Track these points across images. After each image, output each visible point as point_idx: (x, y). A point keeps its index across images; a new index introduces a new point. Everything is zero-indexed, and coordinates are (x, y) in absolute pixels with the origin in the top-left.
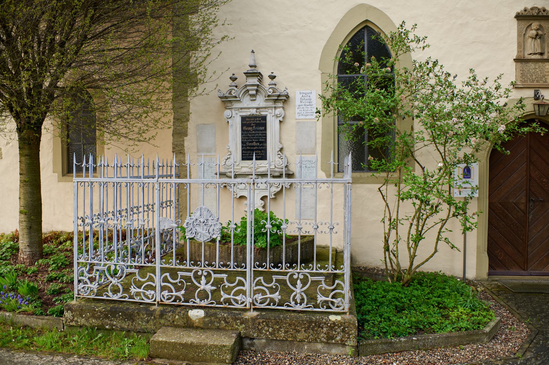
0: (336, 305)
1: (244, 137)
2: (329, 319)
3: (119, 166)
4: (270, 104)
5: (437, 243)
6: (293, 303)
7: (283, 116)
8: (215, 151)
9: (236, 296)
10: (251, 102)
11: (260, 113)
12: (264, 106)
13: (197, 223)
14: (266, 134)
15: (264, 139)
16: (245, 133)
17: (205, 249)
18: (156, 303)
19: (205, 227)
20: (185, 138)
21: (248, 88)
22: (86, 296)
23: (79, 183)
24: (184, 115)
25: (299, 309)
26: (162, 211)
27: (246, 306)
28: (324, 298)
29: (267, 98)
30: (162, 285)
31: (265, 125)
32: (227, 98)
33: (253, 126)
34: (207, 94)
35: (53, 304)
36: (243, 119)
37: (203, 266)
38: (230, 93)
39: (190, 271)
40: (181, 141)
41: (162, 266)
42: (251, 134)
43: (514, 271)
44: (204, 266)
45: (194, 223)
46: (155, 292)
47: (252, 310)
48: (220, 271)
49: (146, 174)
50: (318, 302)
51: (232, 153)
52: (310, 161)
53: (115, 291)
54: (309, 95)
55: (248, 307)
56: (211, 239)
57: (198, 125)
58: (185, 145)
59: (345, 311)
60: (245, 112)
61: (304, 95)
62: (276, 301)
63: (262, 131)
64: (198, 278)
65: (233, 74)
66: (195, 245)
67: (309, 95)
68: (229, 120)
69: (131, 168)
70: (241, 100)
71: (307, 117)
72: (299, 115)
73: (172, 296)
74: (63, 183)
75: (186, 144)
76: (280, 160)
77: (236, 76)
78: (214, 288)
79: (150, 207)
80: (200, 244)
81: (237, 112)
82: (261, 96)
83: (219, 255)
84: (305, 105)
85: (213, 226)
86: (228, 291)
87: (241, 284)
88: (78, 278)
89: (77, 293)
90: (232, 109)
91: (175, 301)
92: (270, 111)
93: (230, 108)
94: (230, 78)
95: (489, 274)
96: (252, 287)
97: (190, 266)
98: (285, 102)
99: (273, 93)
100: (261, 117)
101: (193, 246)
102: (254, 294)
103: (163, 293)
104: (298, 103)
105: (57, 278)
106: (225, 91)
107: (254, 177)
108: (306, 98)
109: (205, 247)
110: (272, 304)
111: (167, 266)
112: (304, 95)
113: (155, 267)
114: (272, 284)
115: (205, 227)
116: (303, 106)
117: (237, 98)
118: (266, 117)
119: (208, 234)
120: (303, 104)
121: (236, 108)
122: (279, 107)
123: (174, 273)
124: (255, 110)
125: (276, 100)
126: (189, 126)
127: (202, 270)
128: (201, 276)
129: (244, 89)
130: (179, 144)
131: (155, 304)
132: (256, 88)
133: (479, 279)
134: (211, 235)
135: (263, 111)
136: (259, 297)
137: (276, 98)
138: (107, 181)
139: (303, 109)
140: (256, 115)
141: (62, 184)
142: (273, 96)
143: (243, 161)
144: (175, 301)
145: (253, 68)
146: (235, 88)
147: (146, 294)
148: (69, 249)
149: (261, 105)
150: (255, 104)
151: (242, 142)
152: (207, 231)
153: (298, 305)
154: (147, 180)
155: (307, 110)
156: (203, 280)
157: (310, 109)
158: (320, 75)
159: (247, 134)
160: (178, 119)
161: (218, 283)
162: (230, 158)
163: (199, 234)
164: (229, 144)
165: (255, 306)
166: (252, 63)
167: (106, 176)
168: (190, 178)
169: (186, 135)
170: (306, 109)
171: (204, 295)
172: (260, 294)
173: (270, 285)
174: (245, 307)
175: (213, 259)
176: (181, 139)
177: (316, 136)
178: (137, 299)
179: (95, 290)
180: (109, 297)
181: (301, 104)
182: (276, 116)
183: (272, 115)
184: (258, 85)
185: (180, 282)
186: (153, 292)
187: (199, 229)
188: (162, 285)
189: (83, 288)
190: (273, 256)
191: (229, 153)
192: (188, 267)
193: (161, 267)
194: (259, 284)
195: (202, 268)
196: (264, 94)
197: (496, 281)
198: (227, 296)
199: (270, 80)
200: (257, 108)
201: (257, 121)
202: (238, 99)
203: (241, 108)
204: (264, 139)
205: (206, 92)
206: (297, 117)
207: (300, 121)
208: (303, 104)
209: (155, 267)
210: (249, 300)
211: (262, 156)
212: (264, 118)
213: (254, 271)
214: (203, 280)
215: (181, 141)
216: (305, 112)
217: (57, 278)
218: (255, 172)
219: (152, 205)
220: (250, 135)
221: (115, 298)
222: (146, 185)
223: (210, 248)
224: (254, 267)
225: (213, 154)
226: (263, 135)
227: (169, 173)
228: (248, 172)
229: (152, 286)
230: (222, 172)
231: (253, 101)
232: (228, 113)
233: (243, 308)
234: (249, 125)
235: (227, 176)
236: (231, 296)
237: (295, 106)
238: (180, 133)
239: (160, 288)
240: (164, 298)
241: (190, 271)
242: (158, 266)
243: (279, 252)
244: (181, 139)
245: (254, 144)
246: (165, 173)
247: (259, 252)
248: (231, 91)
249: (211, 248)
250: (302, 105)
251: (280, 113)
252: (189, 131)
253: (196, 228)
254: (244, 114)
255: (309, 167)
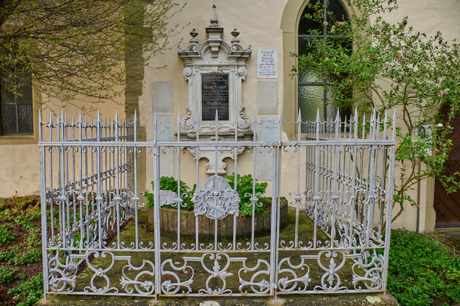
0: (372, 284)
1: (204, 96)
2: (368, 302)
3: (85, 126)
4: (233, 62)
6: (324, 286)
7: (245, 75)
8: (172, 111)
9: (256, 282)
10: (212, 59)
11: (221, 71)
12: (226, 64)
13: (209, 196)
14: (228, 93)
15: (226, 98)
16: (206, 92)
17: (181, 219)
18: (155, 296)
19: (220, 201)
21: (211, 44)
22: (60, 291)
23: (47, 149)
24: (138, 72)
25: (332, 292)
26: (121, 175)
27: (269, 292)
28: (360, 278)
29: (230, 56)
30: (163, 274)
32: (187, 55)
33: (214, 85)
34: (169, 49)
35: (9, 298)
37: (216, 248)
38: (191, 49)
39: (200, 255)
40: (135, 100)
41: (163, 251)
42: (212, 93)
43: (453, 223)
44: (218, 249)
45: (206, 197)
46: (154, 282)
47: (276, 297)
48: (240, 253)
49: (84, 138)
50: (353, 282)
51: (192, 113)
52: (272, 121)
53: (99, 282)
54: (270, 54)
55: (271, 294)
56: (227, 215)
57: (153, 84)
58: (139, 104)
59: (382, 290)
60: (206, 70)
61: (266, 54)
62: (304, 285)
64: (210, 264)
65: (194, 30)
66: (167, 214)
67: (270, 54)
68: (189, 78)
69: (84, 129)
70: (202, 58)
71: (269, 77)
72: (261, 75)
73: (176, 287)
75: (140, 103)
76: (243, 120)
77: (196, 31)
78: (230, 274)
79: (112, 172)
80: (213, 221)
81: (197, 69)
82: (223, 54)
83: (199, 224)
84: (267, 64)
85: (230, 200)
86: (247, 277)
87: (263, 267)
88: (48, 270)
89: (48, 289)
90: (192, 66)
91: (180, 292)
92: (233, 69)
93: (190, 66)
94: (191, 34)
95: (436, 227)
96: (277, 270)
97: (199, 249)
98: (247, 60)
99: (237, 50)
101: (165, 216)
102: (279, 278)
103: (164, 284)
104: (259, 62)
105: (6, 259)
106: (185, 48)
107: (217, 137)
108: (267, 57)
109: (181, 216)
110: (299, 288)
111: (170, 250)
112: (266, 54)
113: (154, 252)
114: (301, 265)
115: (220, 201)
116: (265, 65)
117: (198, 54)
118: (228, 75)
119: (223, 210)
120: (265, 63)
121: (196, 65)
122: (242, 66)
123: (177, 258)
124: (217, 68)
125: (239, 57)
126: (144, 85)
127: (215, 254)
128: (213, 261)
129: (205, 45)
130: (132, 103)
131: (154, 298)
132: (219, 44)
133: (427, 232)
134: (227, 210)
135: (225, 69)
136: (285, 281)
137: (240, 56)
138: (86, 145)
139: (264, 69)
140: (218, 73)
142: (237, 53)
143: (204, 121)
144: (180, 292)
145: (215, 24)
146: (196, 44)
147: (142, 286)
148: (9, 219)
149: (223, 63)
150: (217, 62)
152: (222, 206)
153: (330, 287)
154: (104, 143)
155: (269, 70)
156: (216, 266)
157: (271, 68)
158: (282, 35)
159: (208, 93)
160: (131, 77)
161: (235, 266)
162: (190, 118)
163: (212, 210)
164: (189, 104)
165: (280, 293)
166: (214, 19)
167: (65, 140)
168: (257, 140)
169: (141, 94)
170: (268, 68)
171: (216, 283)
172: (287, 278)
173: (298, 267)
174: (268, 295)
175: (191, 229)
176: (135, 98)
177: (277, 96)
178: (130, 293)
179: (74, 285)
180: (92, 291)
181: (262, 63)
182: (238, 75)
183: (234, 73)
184: (221, 41)
185: (187, 269)
186: (150, 283)
187: (211, 204)
188: (163, 274)
189: (56, 282)
190: (257, 223)
191: (189, 113)
192: (197, 251)
193: (161, 253)
194: (285, 266)
195: (215, 251)
196: (227, 51)
197: (443, 233)
198: (247, 283)
199: (233, 37)
200: (219, 66)
201: (218, 79)
202: (199, 56)
203: (202, 66)
204: (226, 98)
205: (168, 46)
206: (259, 77)
207: (262, 80)
208: (265, 63)
209: (154, 252)
210: (273, 286)
211: (225, 117)
212: (226, 77)
213: (279, 251)
214: (216, 266)
215: (135, 100)
216: (266, 72)
217: (6, 259)
218: (218, 133)
219: (114, 171)
220: (211, 94)
221: (100, 292)
222: (104, 149)
223: (187, 217)
224: (280, 247)
225: (170, 113)
226: (225, 94)
227: (112, 136)
228: (210, 133)
229: (149, 275)
230: (182, 133)
231: (214, 59)
232: (187, 70)
233: (266, 295)
235: (188, 138)
236: (251, 283)
237: (256, 65)
238: (133, 91)
239: (160, 278)
240: (166, 290)
241: (200, 255)
242: (157, 251)
243: (262, 218)
244: (135, 98)
246: (108, 136)
247: (244, 220)
248: (192, 48)
249: (189, 217)
250: (264, 64)
251: (243, 72)
253: (208, 202)
255: (271, 128)
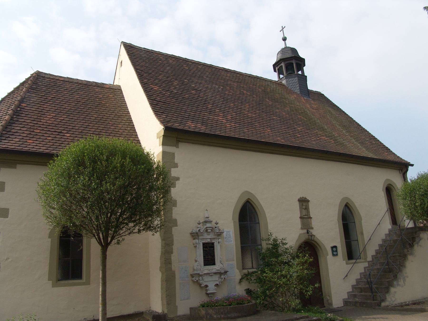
5: (345, 277)
14: (214, 252)
20: (172, 255)
21: (208, 228)
31: (213, 247)
33: (208, 248)
36: (204, 244)
42: (207, 252)
63: (212, 250)
71: (229, 243)
74: (57, 288)
75: (172, 258)
84: (228, 237)
100: (212, 243)
124: (210, 239)
126: (174, 248)
141: (56, 289)
151: (204, 256)
158: (233, 223)
169: (172, 253)
200: (210, 239)
203: (203, 239)
212: (213, 244)
234: (206, 247)
245: (209, 257)
252: (174, 251)
254: (204, 242)
